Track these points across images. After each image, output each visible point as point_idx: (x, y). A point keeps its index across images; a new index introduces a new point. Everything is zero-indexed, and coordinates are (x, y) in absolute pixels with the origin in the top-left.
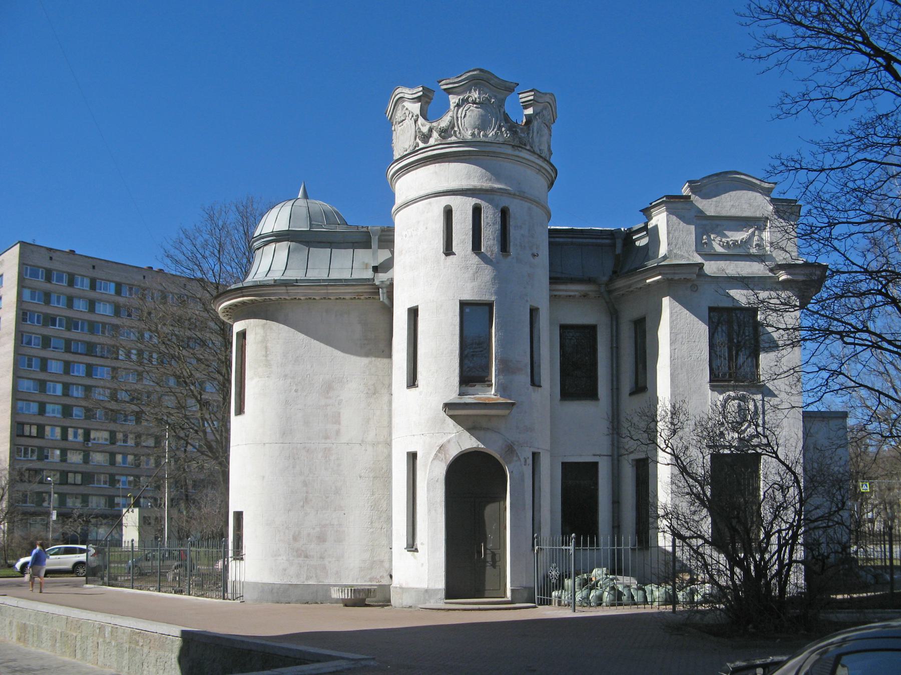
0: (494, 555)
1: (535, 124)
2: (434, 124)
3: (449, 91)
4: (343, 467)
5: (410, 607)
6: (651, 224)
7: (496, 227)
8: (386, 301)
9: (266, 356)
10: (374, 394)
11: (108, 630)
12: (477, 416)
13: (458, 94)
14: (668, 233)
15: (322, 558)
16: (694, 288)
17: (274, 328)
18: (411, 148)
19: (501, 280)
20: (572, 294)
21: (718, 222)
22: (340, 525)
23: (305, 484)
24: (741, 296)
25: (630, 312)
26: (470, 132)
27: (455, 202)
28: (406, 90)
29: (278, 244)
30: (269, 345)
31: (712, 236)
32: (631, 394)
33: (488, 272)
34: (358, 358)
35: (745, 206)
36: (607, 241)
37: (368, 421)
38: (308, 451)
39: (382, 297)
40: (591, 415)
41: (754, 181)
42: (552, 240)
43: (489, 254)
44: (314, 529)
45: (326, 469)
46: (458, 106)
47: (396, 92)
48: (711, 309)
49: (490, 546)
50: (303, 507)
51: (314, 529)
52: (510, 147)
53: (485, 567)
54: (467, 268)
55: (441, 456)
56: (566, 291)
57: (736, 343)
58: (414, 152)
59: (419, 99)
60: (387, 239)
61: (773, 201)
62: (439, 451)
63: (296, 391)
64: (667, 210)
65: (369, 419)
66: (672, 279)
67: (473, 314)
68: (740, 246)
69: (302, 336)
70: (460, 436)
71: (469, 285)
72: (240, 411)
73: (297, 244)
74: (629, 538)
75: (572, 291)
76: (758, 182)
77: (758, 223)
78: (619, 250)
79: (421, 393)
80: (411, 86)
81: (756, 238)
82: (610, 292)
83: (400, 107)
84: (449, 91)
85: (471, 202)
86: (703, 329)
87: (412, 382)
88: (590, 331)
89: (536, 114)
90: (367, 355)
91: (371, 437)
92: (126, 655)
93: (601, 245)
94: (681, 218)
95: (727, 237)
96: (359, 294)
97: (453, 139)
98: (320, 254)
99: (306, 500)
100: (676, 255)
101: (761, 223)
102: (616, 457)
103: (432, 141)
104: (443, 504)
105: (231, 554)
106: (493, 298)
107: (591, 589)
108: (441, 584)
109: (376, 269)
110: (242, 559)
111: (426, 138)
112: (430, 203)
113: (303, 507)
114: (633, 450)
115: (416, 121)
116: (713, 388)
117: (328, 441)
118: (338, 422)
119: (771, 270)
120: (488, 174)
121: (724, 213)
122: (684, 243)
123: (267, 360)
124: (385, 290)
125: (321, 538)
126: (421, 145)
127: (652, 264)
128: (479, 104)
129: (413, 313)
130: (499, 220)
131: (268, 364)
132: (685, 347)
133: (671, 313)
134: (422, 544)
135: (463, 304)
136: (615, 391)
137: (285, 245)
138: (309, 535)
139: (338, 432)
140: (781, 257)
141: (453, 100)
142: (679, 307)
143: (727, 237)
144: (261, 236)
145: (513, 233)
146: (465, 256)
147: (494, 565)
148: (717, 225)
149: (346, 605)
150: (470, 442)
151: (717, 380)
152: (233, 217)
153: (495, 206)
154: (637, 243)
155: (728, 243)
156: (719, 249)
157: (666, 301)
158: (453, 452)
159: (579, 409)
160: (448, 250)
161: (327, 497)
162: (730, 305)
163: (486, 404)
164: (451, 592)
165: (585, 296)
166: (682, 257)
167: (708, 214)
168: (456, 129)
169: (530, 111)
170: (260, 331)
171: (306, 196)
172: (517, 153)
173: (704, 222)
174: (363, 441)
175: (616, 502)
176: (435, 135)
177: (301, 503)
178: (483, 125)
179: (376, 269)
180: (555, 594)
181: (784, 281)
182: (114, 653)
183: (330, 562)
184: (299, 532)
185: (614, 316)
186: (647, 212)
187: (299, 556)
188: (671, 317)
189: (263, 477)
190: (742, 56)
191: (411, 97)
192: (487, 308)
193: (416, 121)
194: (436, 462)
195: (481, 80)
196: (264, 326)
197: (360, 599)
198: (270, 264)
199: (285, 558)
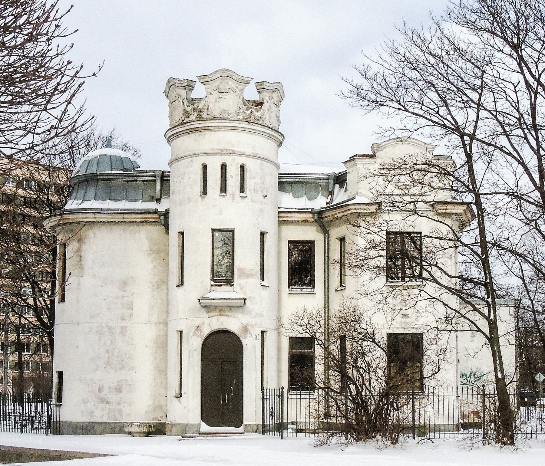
18: (181, 121)
20: (296, 219)
45: (123, 342)
52: (247, 123)
72: (63, 299)
117: (124, 322)
125: (119, 390)
136: (327, 287)
139: (131, 315)
158: (206, 331)
187: (103, 402)
196: (173, 194)
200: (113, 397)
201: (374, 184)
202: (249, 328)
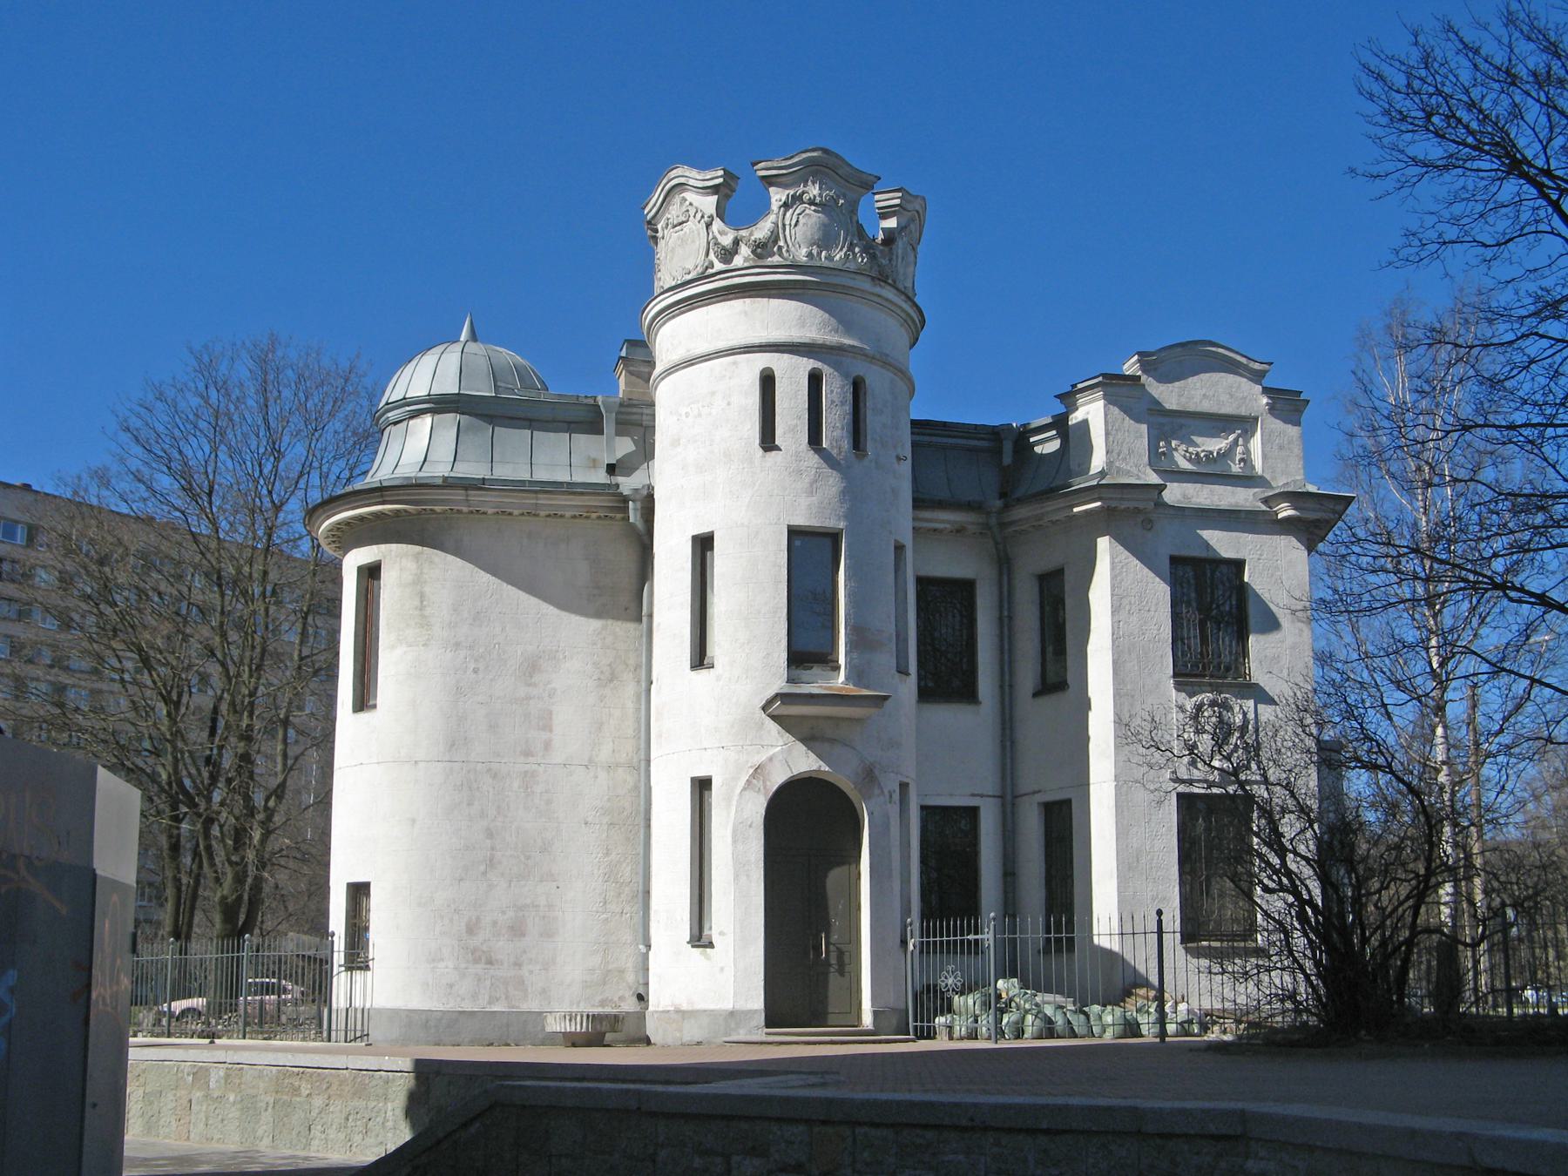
0: (841, 954)
1: (900, 245)
2: (743, 233)
3: (769, 181)
4: (552, 802)
5: (699, 1043)
6: (1076, 418)
7: (842, 406)
8: (640, 525)
9: (422, 608)
10: (611, 681)
11: (217, 1074)
12: (817, 718)
13: (785, 186)
14: (1107, 434)
15: (518, 965)
16: (1148, 524)
17: (436, 560)
18: (699, 269)
19: (852, 496)
21: (1182, 421)
22: (550, 906)
23: (490, 834)
24: (1223, 543)
25: (1031, 562)
26: (804, 251)
27: (780, 364)
28: (694, 173)
29: (437, 417)
30: (427, 589)
31: (1174, 443)
32: (1035, 695)
33: (833, 483)
34: (583, 620)
35: (1224, 398)
36: (984, 444)
37: (600, 726)
38: (495, 776)
39: (634, 516)
40: (968, 726)
41: (1238, 358)
42: (918, 438)
43: (834, 452)
44: (504, 913)
46: (786, 206)
47: (673, 174)
48: (1175, 561)
49: (834, 937)
50: (484, 873)
51: (504, 913)
53: (826, 974)
54: (800, 472)
55: (758, 783)
56: (930, 521)
57: (1212, 615)
58: (702, 277)
59: (715, 189)
60: (637, 421)
61: (1267, 391)
62: (753, 776)
63: (476, 671)
64: (1105, 397)
65: (602, 724)
66: (1115, 509)
67: (809, 553)
68: (1215, 460)
69: (485, 577)
70: (789, 751)
71: (804, 501)
72: (363, 701)
73: (473, 419)
74: (1033, 928)
75: (943, 521)
76: (1244, 360)
77: (1244, 424)
78: (1007, 459)
79: (718, 678)
80: (702, 166)
81: (1240, 449)
82: (1003, 525)
83: (677, 199)
84: (769, 181)
85: (806, 365)
86: (1161, 591)
87: (700, 658)
88: (963, 590)
89: (901, 228)
90: (598, 615)
91: (604, 755)
92: (267, 1117)
93: (971, 450)
94: (1126, 410)
95: (1197, 445)
96: (590, 509)
97: (776, 259)
98: (514, 439)
99: (491, 863)
100: (1119, 470)
101: (1248, 426)
102: (1009, 797)
103: (738, 261)
104: (762, 864)
105: (339, 958)
106: (842, 525)
107: (1002, 1011)
108: (757, 1002)
109: (611, 469)
110: (367, 968)
111: (728, 254)
112: (735, 363)
113: (484, 873)
114: (1040, 783)
115: (708, 225)
116: (1179, 687)
117: (531, 759)
118: (548, 727)
119: (1266, 501)
120: (833, 321)
121: (1191, 408)
122: (1131, 452)
123: (423, 616)
124: (639, 505)
125: (517, 930)
126: (719, 266)
127: (1079, 484)
128: (821, 206)
129: (703, 545)
130: (850, 397)
131: (424, 622)
132: (1134, 618)
133: (1113, 563)
134: (721, 933)
135: (794, 532)
137: (450, 419)
138: (495, 923)
139: (547, 746)
140: (1280, 483)
141: (777, 196)
142: (1124, 554)
143: (1197, 445)
144: (405, 402)
145: (872, 422)
146: (797, 454)
147: (841, 972)
148: (1181, 426)
149: (574, 1045)
150: (805, 762)
151: (1186, 676)
152: (243, 371)
153: (845, 375)
154: (1038, 449)
155: (1197, 454)
156: (1184, 465)
157: (1104, 544)
158: (778, 778)
159: (948, 716)
160: (768, 441)
161: (528, 858)
162: (1203, 554)
163: (842, 696)
164: (775, 1017)
165: (960, 530)
166: (1128, 473)
167: (1168, 406)
168: (781, 243)
169: (892, 223)
170: (411, 565)
171: (474, 337)
172: (877, 290)
173: (1161, 420)
174: (590, 761)
175: (1010, 874)
176: (745, 250)
177: (482, 868)
178: (825, 240)
179: (611, 469)
180: (940, 1020)
181: (1288, 519)
182: (234, 1113)
183: (531, 972)
184: (478, 919)
185: (1004, 565)
186: (1069, 399)
187: (476, 961)
188: (1113, 568)
189: (414, 821)
190: (1352, 170)
191: (700, 184)
192: (828, 542)
193: (708, 225)
194: (749, 794)
195: (823, 167)
196: (417, 557)
197: (601, 1030)
198: (414, 450)
199: (451, 965)
200: (503, 948)
201: (1425, 363)
202: (877, 772)
